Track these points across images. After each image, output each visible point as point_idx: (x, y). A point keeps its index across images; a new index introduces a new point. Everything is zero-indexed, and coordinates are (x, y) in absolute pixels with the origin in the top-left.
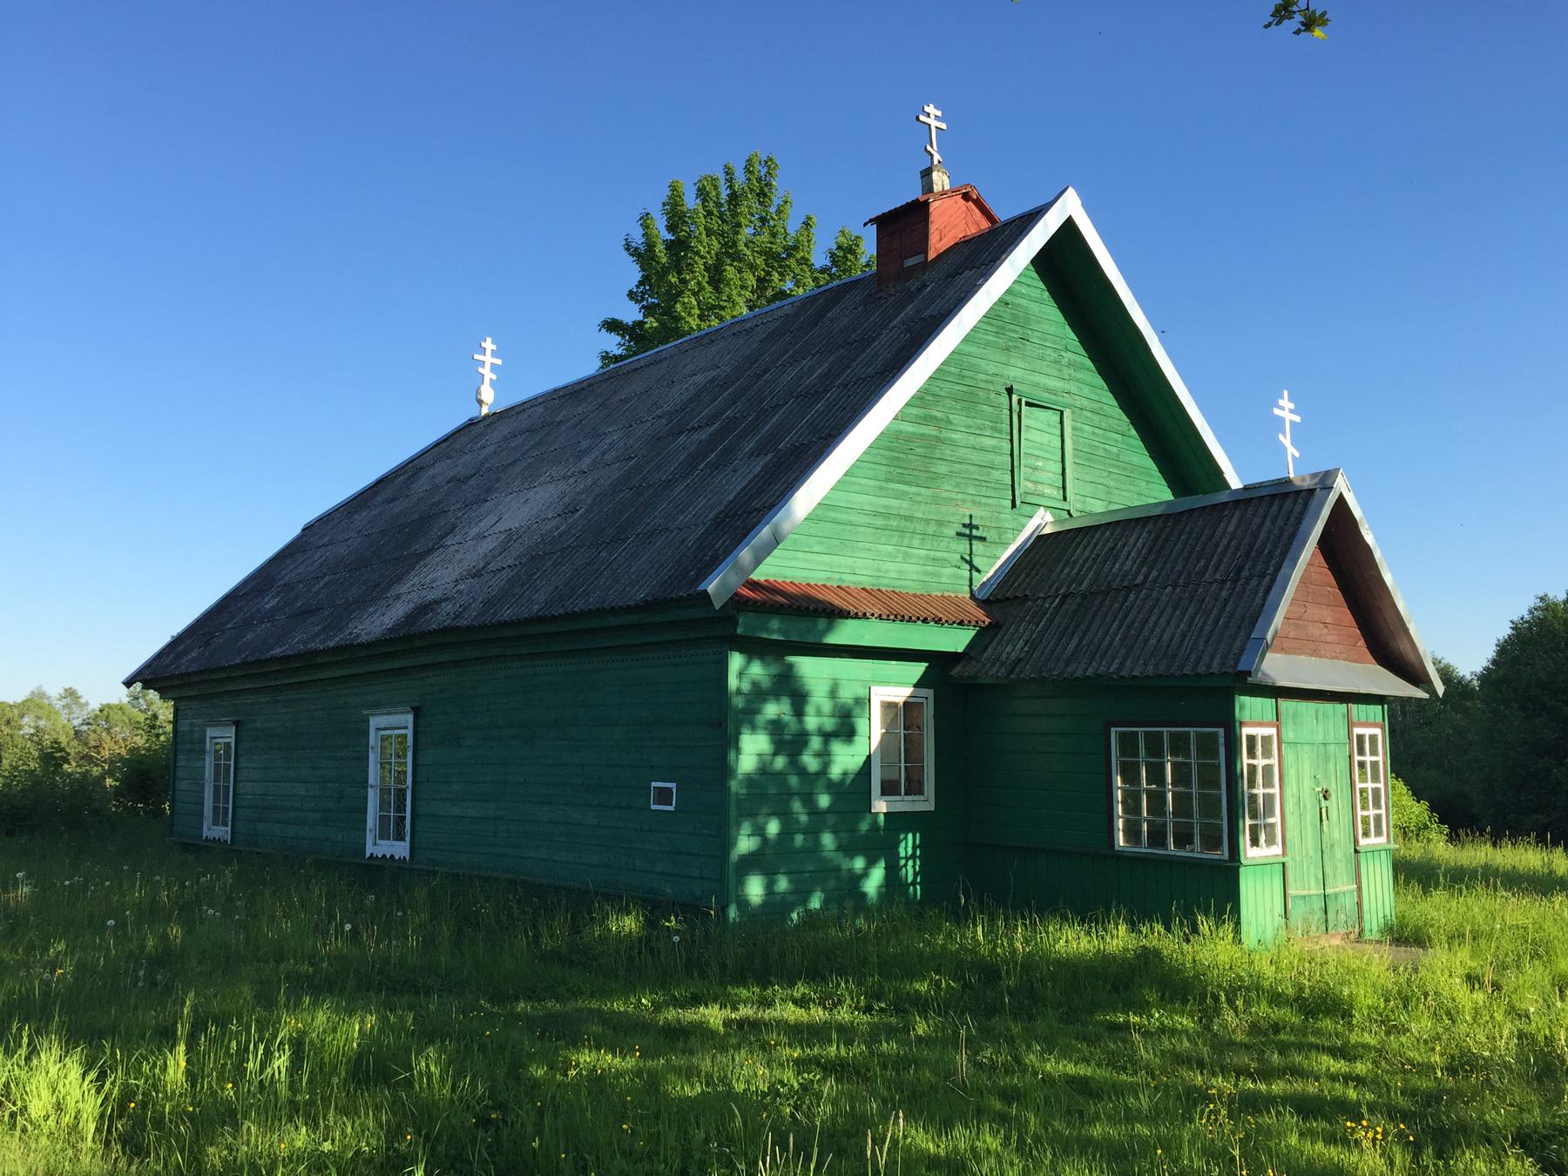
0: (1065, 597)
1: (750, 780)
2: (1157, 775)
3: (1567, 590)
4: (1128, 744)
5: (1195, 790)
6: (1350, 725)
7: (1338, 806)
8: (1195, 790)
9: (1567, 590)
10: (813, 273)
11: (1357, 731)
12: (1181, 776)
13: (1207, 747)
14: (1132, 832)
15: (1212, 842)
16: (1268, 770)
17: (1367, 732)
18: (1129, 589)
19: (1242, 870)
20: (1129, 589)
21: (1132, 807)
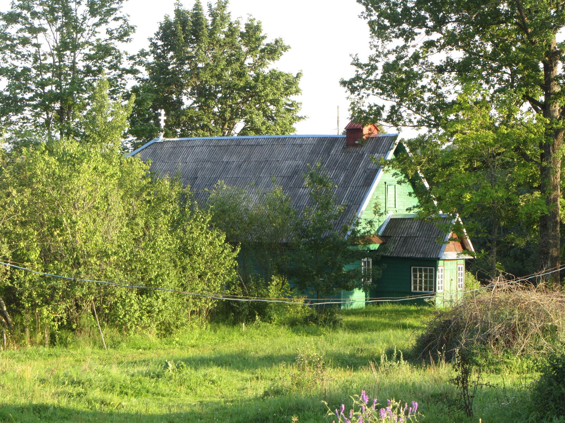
0: (401, 237)
1: (255, 315)
2: (421, 276)
3: (357, 1)
4: (415, 271)
5: (428, 279)
6: (457, 265)
7: (454, 282)
8: (428, 279)
9: (357, 1)
10: (232, 42)
11: (459, 266)
12: (426, 277)
13: (431, 271)
14: (415, 288)
15: (431, 290)
16: (442, 287)
17: (460, 266)
18: (416, 237)
19: (441, 263)
20: (416, 237)
21: (415, 282)
